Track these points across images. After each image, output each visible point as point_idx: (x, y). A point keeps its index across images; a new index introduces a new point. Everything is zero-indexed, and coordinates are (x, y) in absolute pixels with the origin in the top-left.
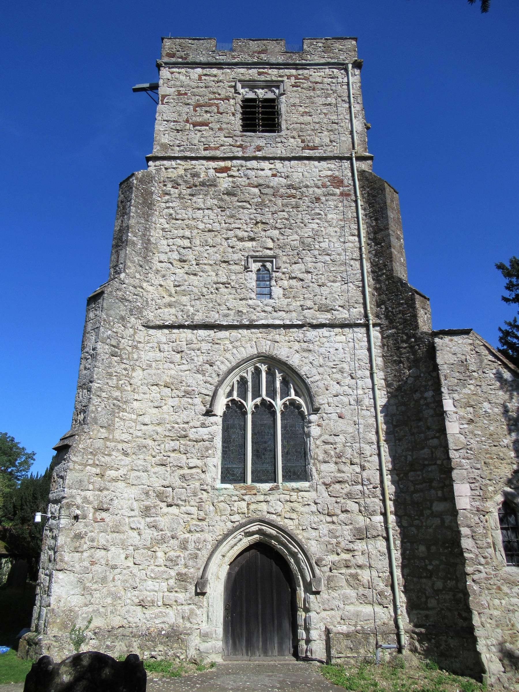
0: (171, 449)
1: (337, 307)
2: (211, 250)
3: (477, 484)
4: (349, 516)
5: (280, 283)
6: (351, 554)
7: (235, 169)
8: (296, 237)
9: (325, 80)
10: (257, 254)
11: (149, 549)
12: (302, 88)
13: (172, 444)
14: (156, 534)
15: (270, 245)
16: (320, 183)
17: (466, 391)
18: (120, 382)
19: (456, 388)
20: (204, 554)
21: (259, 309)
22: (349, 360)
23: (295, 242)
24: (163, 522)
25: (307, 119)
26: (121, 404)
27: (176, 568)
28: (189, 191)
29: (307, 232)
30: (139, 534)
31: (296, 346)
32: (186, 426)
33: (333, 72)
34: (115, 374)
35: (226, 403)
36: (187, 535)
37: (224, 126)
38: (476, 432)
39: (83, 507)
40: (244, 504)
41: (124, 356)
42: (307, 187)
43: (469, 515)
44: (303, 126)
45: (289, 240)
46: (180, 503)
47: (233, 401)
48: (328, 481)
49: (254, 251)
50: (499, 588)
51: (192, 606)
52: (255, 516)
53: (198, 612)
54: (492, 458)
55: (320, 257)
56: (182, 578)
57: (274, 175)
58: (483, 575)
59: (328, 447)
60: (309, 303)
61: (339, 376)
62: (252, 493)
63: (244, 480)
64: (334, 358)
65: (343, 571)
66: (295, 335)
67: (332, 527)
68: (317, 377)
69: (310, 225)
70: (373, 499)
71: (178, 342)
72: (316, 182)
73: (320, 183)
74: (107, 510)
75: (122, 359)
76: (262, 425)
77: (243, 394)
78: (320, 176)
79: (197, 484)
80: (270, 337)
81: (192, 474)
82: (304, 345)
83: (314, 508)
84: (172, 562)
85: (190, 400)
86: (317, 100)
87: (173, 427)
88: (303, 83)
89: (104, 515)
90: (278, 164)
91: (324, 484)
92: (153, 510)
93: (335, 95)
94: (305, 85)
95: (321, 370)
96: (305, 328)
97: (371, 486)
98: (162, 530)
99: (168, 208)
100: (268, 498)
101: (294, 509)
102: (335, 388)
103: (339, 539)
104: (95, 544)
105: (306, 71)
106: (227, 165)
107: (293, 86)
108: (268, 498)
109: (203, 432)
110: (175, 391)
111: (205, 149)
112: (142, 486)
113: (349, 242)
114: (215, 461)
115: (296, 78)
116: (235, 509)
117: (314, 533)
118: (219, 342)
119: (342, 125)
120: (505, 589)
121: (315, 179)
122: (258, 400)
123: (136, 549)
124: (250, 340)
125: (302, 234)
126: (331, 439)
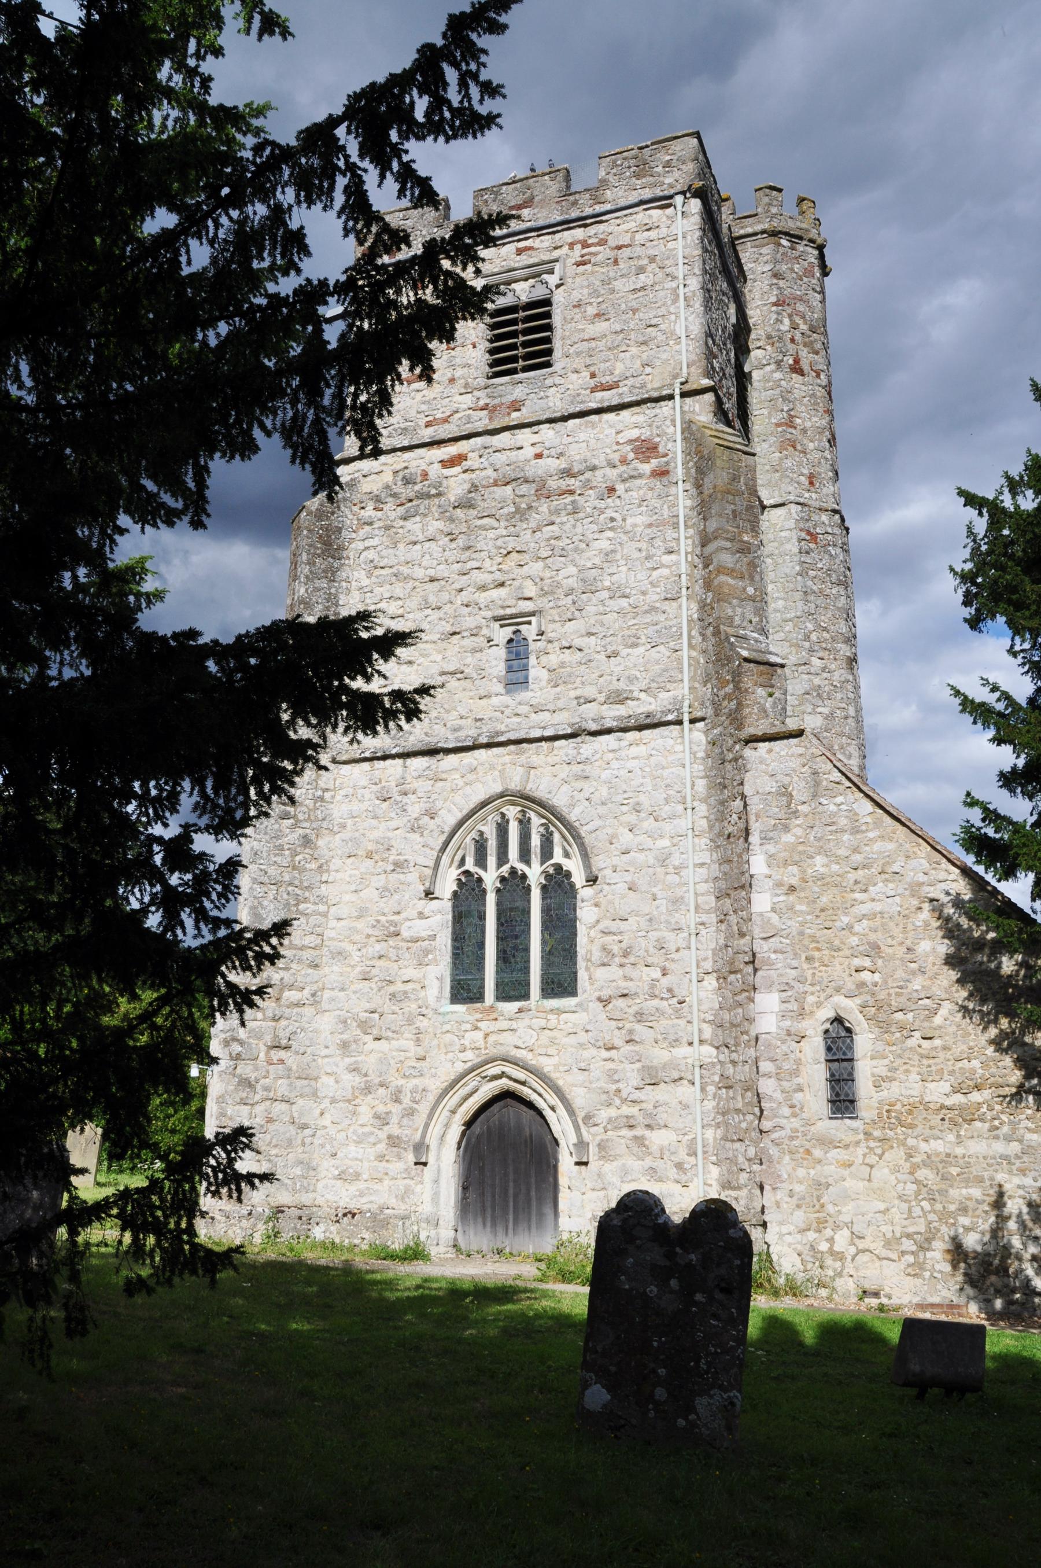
0: (377, 955)
1: (636, 694)
2: (435, 615)
3: (789, 993)
4: (637, 1048)
5: (544, 659)
6: (637, 1108)
7: (475, 455)
8: (572, 570)
9: (638, 236)
10: (509, 611)
11: (349, 1101)
12: (594, 265)
13: (378, 947)
14: (358, 1079)
15: (531, 590)
16: (616, 457)
17: (788, 838)
18: (297, 858)
19: (771, 834)
20: (424, 1109)
21: (508, 712)
22: (650, 788)
23: (570, 580)
24: (370, 1062)
25: (602, 326)
26: (299, 892)
27: (386, 1128)
28: (401, 510)
29: (591, 558)
30: (337, 1082)
31: (564, 771)
32: (395, 918)
33: (650, 216)
34: (286, 847)
35: (455, 877)
36: (401, 1082)
37: (459, 373)
38: (798, 907)
39: (249, 1044)
40: (479, 1035)
41: (301, 817)
42: (594, 469)
43: (774, 1042)
44: (593, 344)
45: (560, 577)
46: (390, 1034)
47: (467, 873)
48: (605, 994)
49: (503, 607)
50: (808, 1152)
51: (407, 1181)
52: (493, 1052)
53: (418, 1189)
54: (818, 949)
55: (611, 602)
56: (394, 1141)
57: (539, 456)
58: (787, 1132)
59: (609, 939)
60: (590, 692)
61: (632, 818)
62: (492, 1017)
63: (479, 997)
64: (624, 787)
65: (625, 1132)
66: (562, 753)
67: (610, 1065)
68: (597, 823)
69: (596, 545)
70: (676, 1021)
71: (383, 784)
72: (611, 456)
73: (616, 457)
74: (287, 1048)
75: (298, 821)
76: (511, 909)
77: (481, 861)
78: (618, 443)
79: (414, 1006)
80: (523, 759)
81: (405, 992)
82: (577, 768)
83: (583, 1037)
84: (382, 1119)
85: (401, 876)
86: (618, 284)
87: (378, 921)
88: (595, 254)
89: (282, 1054)
90: (547, 432)
91: (600, 1000)
92: (354, 1046)
93: (654, 265)
94: (600, 257)
95: (602, 810)
96: (579, 740)
97: (675, 1000)
98: (366, 1075)
99: (367, 548)
100: (514, 1025)
101: (545, 1041)
102: (626, 838)
103: (621, 1085)
104: (271, 1095)
105: (601, 227)
106: (460, 451)
107: (578, 264)
108: (514, 1025)
109: (420, 928)
110: (380, 863)
111: (428, 425)
112: (338, 1012)
113: (663, 566)
114: (439, 971)
115: (585, 245)
116: (467, 1043)
117: (581, 1077)
118: (444, 776)
119: (662, 327)
120: (817, 1153)
121: (608, 451)
122: (505, 869)
123: (333, 1101)
124: (492, 767)
125: (582, 563)
126: (614, 926)
